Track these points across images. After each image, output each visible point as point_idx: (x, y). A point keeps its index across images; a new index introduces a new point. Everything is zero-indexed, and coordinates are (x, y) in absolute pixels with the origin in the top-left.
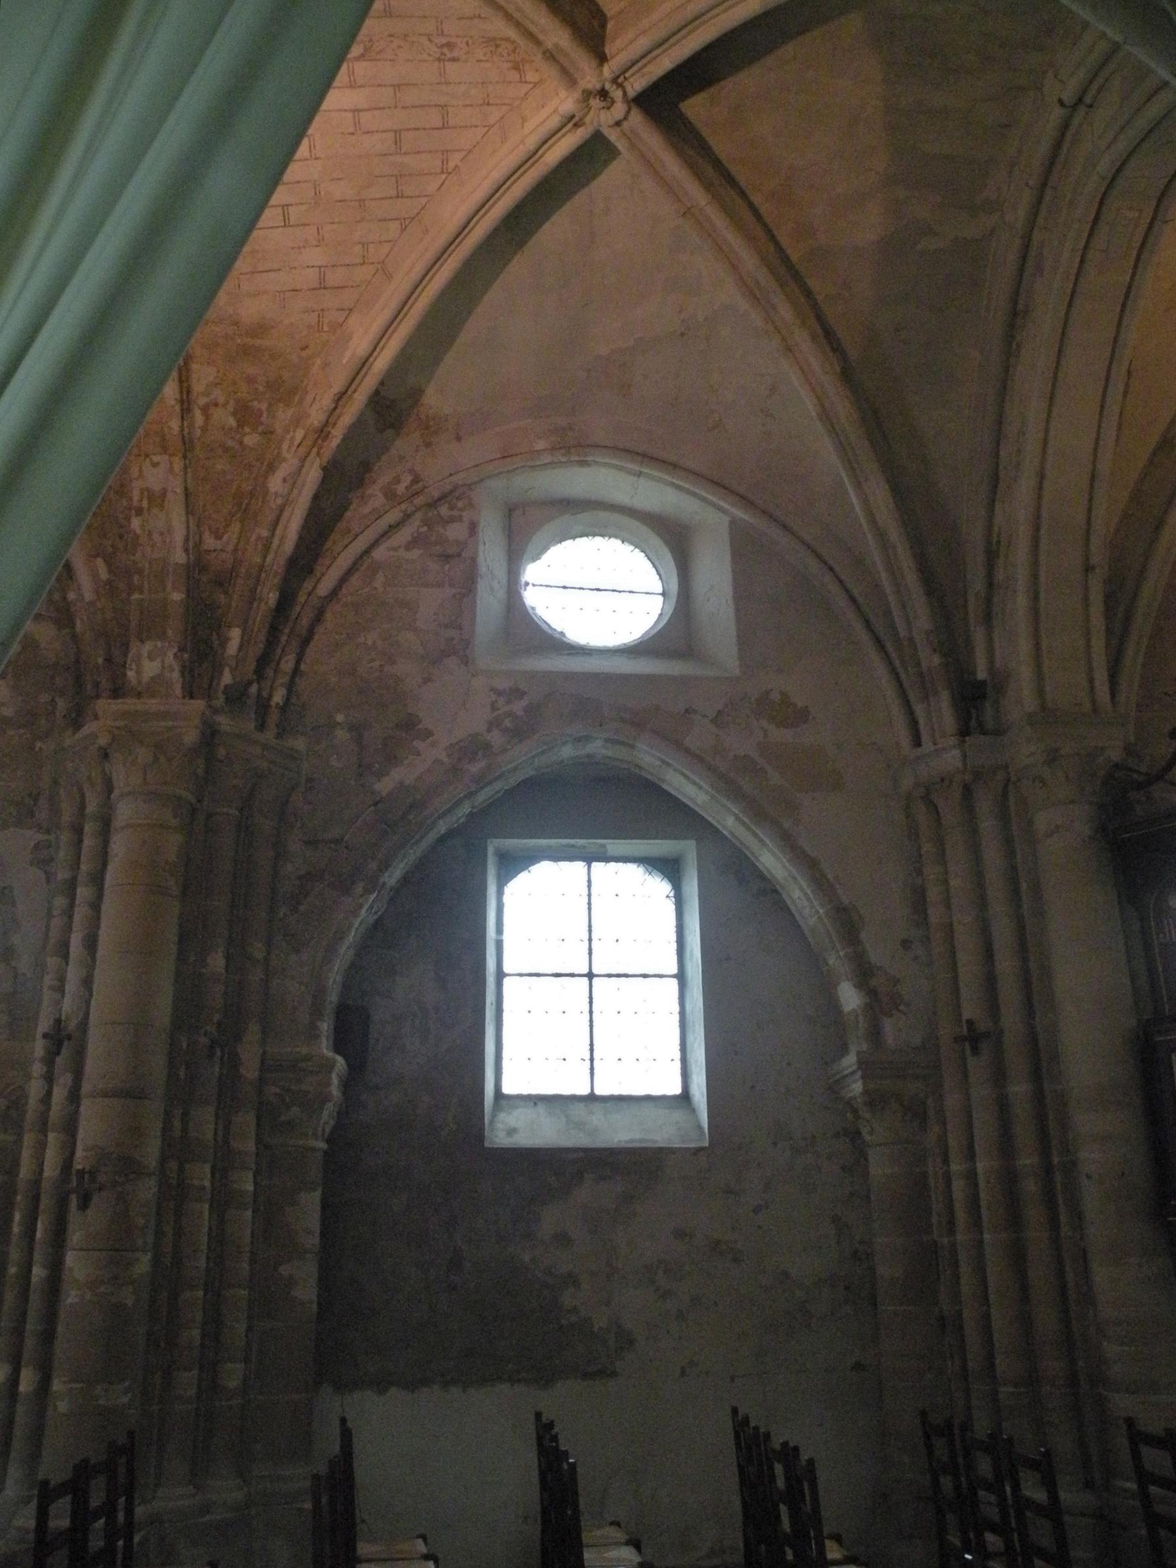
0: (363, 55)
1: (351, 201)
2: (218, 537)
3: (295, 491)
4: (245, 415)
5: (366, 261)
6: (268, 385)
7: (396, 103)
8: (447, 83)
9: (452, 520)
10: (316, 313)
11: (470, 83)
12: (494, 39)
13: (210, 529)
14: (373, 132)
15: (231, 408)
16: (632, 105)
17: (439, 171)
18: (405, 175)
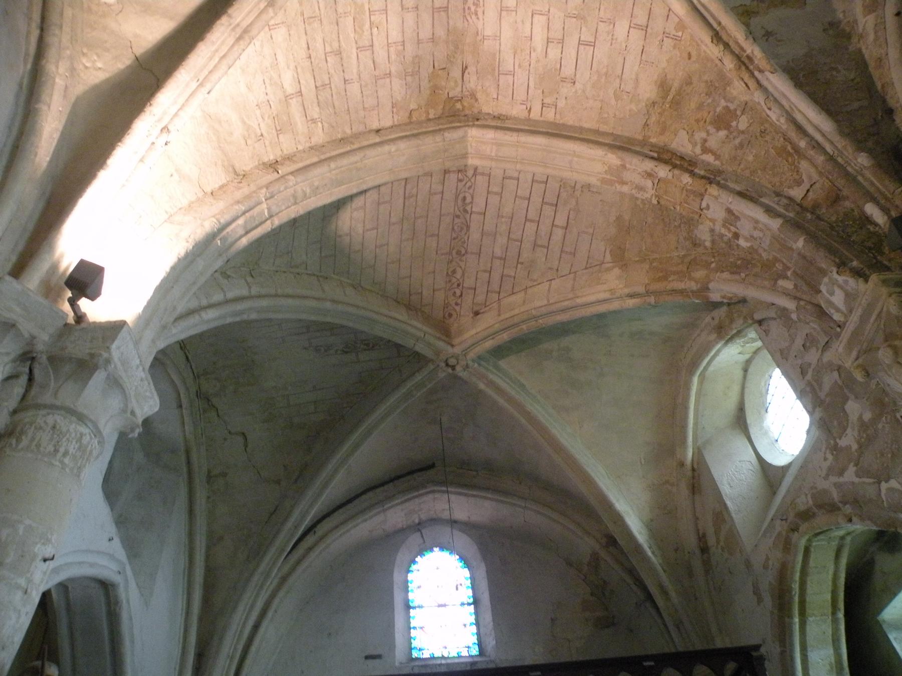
2: (799, 183)
3: (784, 102)
4: (723, 121)
6: (708, 94)
13: (789, 188)
15: (712, 130)
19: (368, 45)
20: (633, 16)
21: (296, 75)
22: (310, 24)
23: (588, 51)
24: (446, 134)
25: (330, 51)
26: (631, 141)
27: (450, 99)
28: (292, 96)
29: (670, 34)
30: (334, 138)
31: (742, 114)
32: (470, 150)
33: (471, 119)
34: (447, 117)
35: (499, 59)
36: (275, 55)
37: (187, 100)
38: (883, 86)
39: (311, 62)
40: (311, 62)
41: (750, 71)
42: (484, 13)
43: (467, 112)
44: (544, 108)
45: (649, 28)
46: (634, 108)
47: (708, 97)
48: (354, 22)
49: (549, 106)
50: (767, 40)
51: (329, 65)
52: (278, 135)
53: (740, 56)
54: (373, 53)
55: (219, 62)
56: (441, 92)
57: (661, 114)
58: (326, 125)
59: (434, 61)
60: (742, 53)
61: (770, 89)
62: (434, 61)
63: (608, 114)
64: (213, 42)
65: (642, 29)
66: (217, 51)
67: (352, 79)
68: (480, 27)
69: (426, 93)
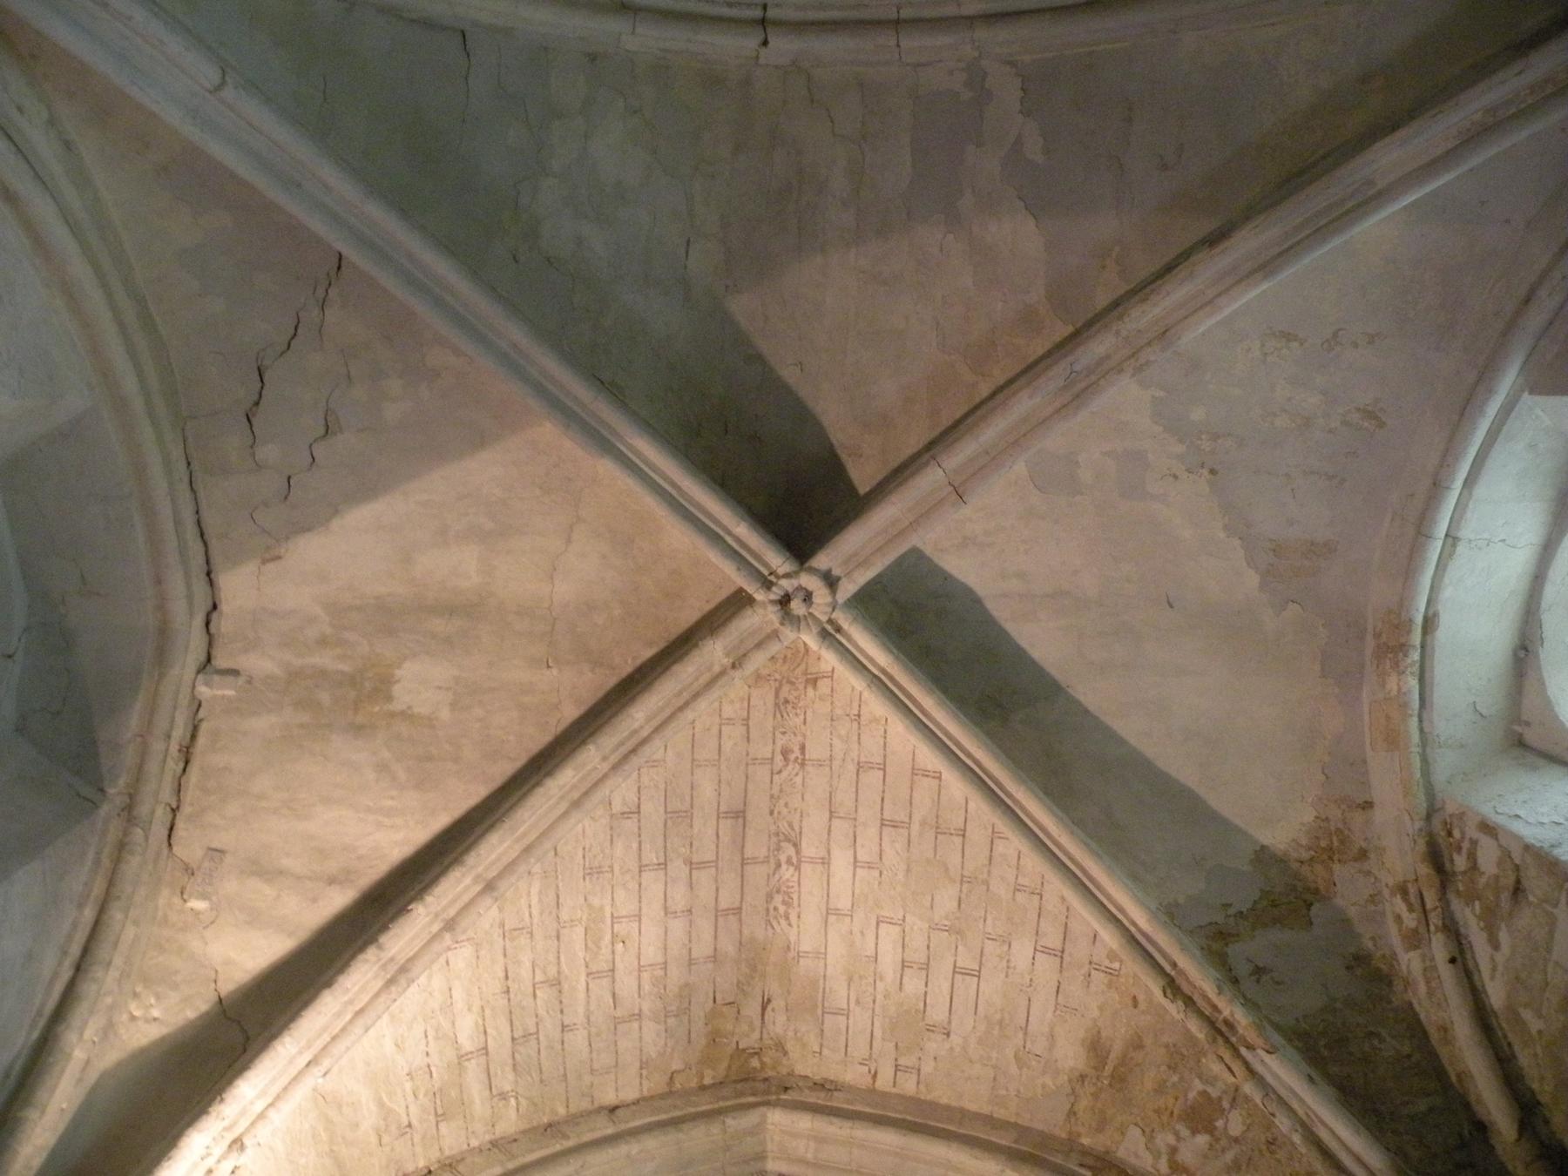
0: (795, 845)
1: (961, 891)
3: (1295, 1105)
4: (1201, 1116)
5: (1038, 891)
6: (1172, 1068)
7: (851, 819)
8: (831, 758)
9: (1472, 856)
10: (1093, 972)
11: (831, 734)
12: (777, 705)
14: (881, 850)
15: (1185, 1132)
16: (807, 565)
17: (937, 781)
18: (937, 822)
19: (606, 969)
20: (1040, 933)
21: (480, 1022)
22: (512, 939)
23: (966, 986)
24: (729, 1121)
25: (542, 980)
26: (1045, 1140)
27: (739, 1052)
28: (470, 1056)
29: (1100, 965)
30: (535, 1124)
31: (1232, 1107)
32: (770, 1146)
33: (774, 1089)
34: (735, 1082)
35: (824, 989)
36: (450, 989)
37: (285, 1089)
38: (1458, 1076)
39: (509, 1000)
40: (509, 1000)
41: (1233, 1045)
42: (799, 917)
43: (770, 1073)
44: (898, 1073)
45: (1066, 953)
46: (1050, 1083)
47: (1171, 1072)
48: (586, 935)
49: (907, 1070)
50: (1258, 981)
51: (539, 1002)
52: (437, 1123)
53: (1214, 1019)
54: (614, 982)
55: (351, 1021)
56: (725, 1040)
57: (1095, 1096)
58: (523, 1102)
59: (715, 992)
60: (1216, 1015)
61: (1269, 1079)
62: (715, 992)
63: (1007, 1090)
64: (347, 988)
65: (1056, 955)
66: (351, 1002)
67: (575, 1024)
68: (793, 939)
69: (701, 1042)
